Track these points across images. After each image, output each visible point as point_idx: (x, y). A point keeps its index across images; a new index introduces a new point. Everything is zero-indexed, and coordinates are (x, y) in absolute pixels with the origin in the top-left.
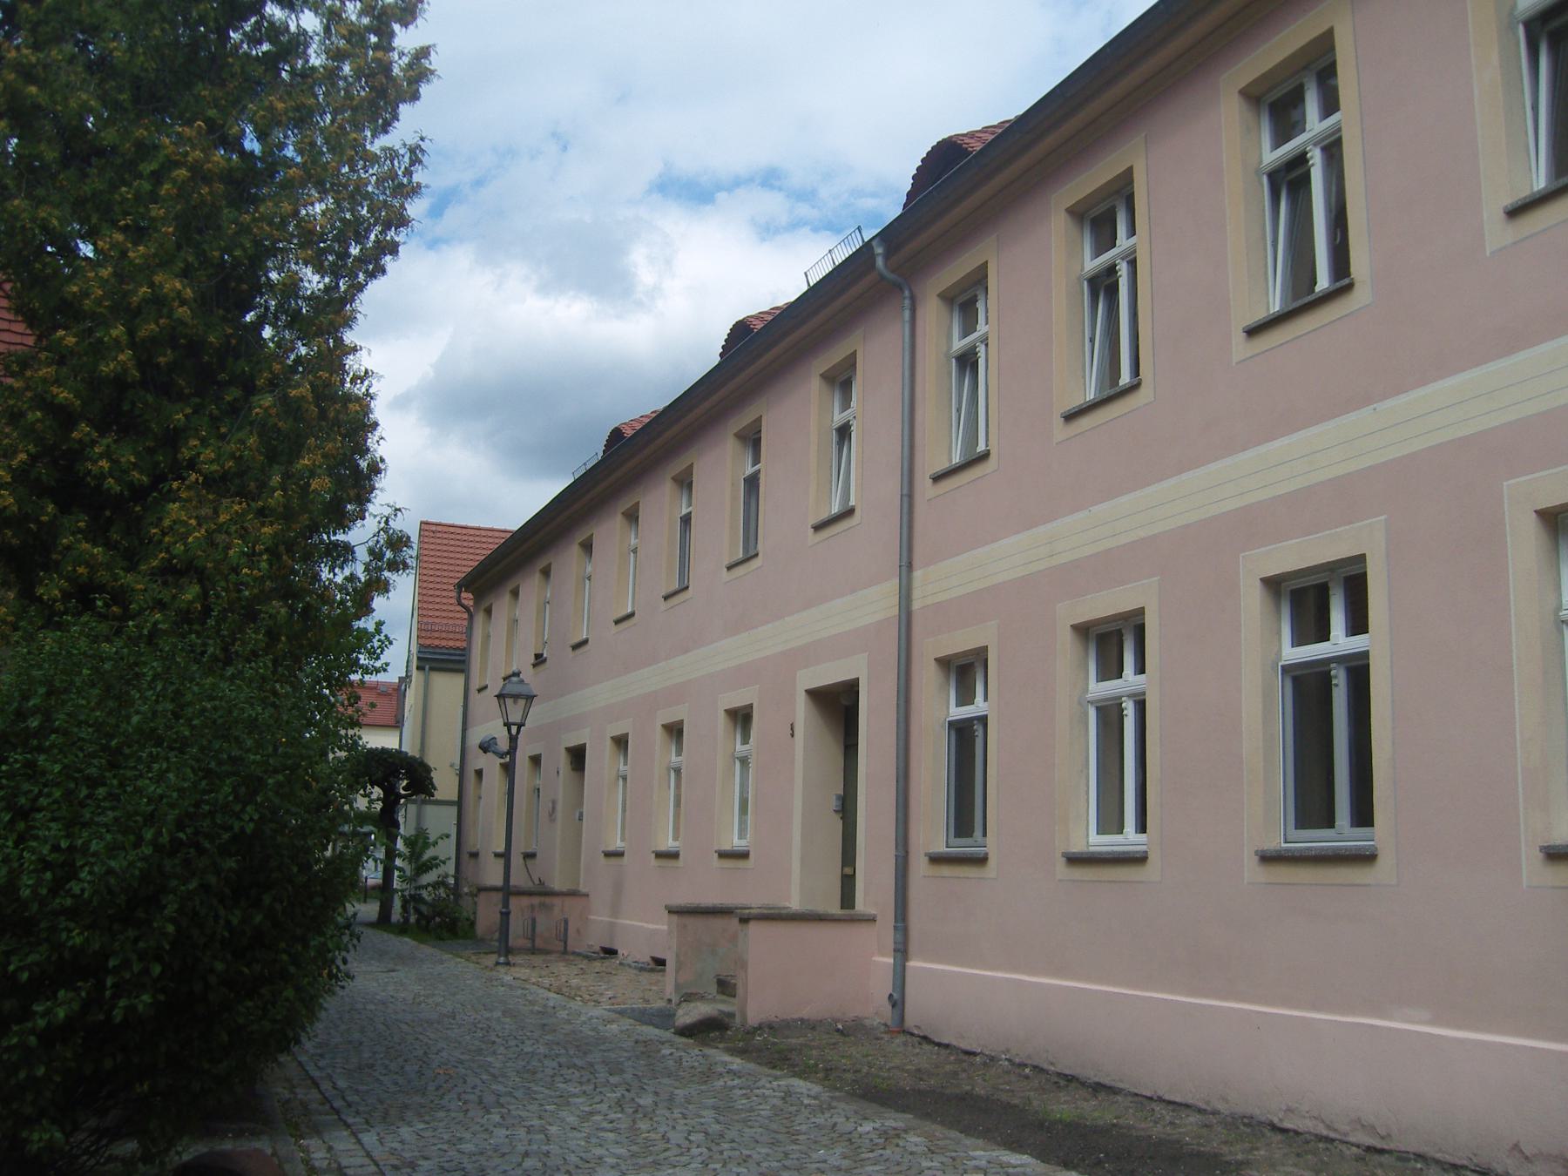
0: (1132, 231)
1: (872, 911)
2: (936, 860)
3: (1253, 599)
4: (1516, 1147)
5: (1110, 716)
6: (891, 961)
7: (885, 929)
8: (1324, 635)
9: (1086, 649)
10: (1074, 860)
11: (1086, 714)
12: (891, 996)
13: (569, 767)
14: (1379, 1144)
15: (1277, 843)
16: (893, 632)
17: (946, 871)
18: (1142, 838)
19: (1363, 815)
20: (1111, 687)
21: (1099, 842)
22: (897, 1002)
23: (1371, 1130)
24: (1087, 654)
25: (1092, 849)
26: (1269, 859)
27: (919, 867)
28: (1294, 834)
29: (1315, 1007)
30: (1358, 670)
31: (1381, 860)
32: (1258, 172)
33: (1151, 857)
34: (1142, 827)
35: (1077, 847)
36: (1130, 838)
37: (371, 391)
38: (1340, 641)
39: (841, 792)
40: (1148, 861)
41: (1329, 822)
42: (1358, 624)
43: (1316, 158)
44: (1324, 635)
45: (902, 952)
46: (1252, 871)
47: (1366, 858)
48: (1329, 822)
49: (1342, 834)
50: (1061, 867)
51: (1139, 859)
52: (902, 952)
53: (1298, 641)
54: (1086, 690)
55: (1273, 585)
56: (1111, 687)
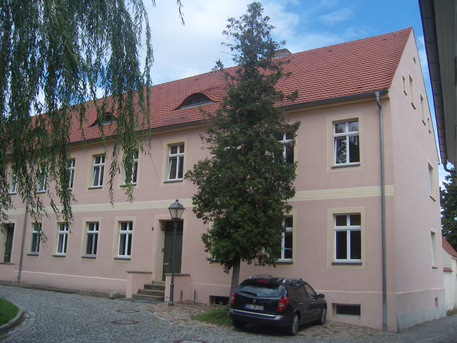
0: (74, 166)
1: (14, 263)
2: (28, 255)
3: (84, 224)
4: (108, 290)
5: (61, 236)
6: (18, 271)
7: (18, 267)
8: (93, 230)
9: (88, 225)
10: (54, 256)
11: (58, 235)
12: (18, 277)
13: (160, 229)
14: (93, 291)
15: (84, 255)
16: (24, 217)
17: (30, 257)
18: (65, 253)
19: (95, 253)
20: (124, 232)
21: (58, 254)
22: (19, 278)
23: (92, 290)
24: (59, 227)
25: (118, 257)
26: (83, 257)
27: (25, 256)
28: (86, 254)
29: (87, 276)
30: (97, 235)
31: (66, 257)
32: (93, 166)
33: (66, 256)
34: (65, 252)
35: (55, 254)
36: (63, 253)
37: (231, 50)
38: (95, 231)
39: (6, 242)
40: (293, 264)
41: (91, 253)
42: (97, 229)
43: (100, 168)
44: (93, 230)
45: (20, 269)
46: (81, 259)
47: (95, 258)
48: (91, 253)
49: (92, 255)
50: (52, 257)
51: (65, 257)
52: (20, 269)
53: (89, 230)
54: (32, 232)
55: (87, 223)
56: (124, 232)
